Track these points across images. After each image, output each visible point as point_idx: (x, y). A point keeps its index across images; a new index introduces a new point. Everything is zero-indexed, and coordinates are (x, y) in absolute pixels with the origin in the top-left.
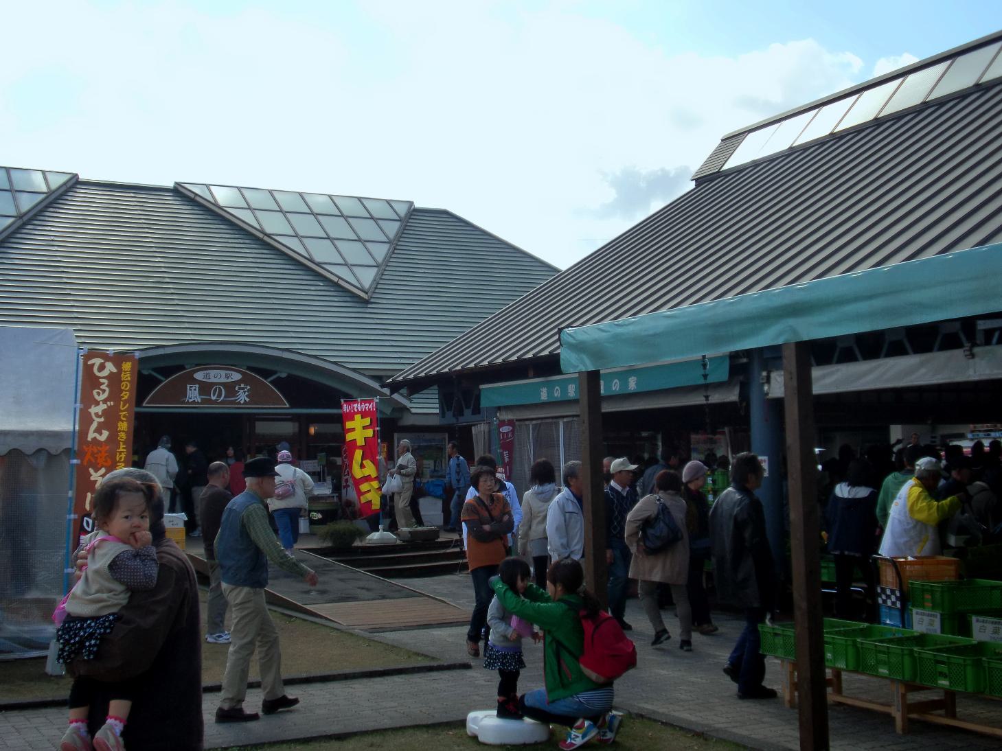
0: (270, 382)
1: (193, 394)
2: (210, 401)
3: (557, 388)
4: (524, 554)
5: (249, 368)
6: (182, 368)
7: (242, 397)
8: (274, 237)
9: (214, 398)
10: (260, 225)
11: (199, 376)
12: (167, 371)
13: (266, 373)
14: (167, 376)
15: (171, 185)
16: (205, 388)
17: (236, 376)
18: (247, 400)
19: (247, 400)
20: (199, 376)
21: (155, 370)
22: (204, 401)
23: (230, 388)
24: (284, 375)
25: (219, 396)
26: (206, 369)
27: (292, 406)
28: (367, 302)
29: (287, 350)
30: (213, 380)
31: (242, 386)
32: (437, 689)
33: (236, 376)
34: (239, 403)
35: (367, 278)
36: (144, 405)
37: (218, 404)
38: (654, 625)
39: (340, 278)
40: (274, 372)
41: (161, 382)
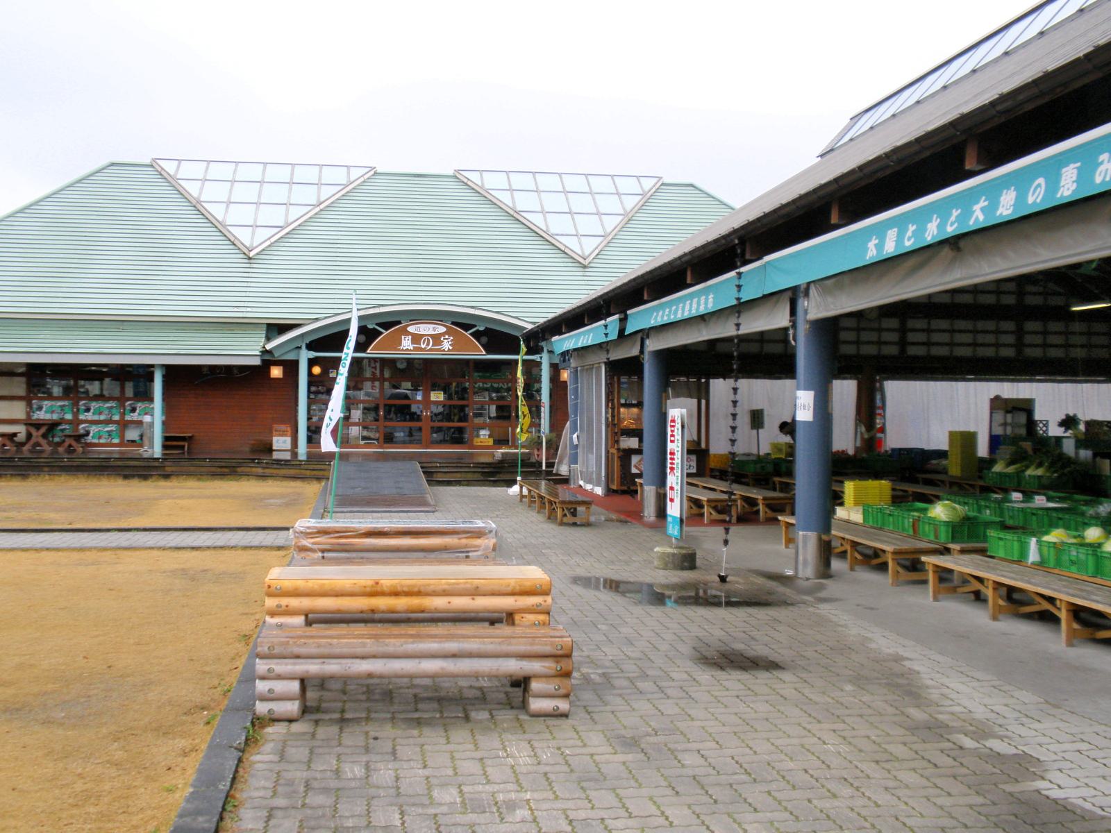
0: (471, 334)
1: (407, 343)
2: (421, 349)
3: (1041, 181)
4: (472, 730)
5: (453, 323)
6: (399, 323)
7: (446, 345)
8: (556, 237)
9: (423, 346)
10: (547, 226)
11: (411, 329)
12: (387, 326)
13: (466, 327)
14: (386, 330)
15: (451, 172)
16: (416, 338)
17: (442, 329)
18: (451, 348)
19: (451, 348)
20: (411, 329)
21: (377, 324)
22: (415, 349)
23: (437, 338)
24: (482, 329)
25: (428, 345)
26: (417, 324)
27: (488, 352)
28: (585, 267)
29: (472, 307)
30: (422, 332)
31: (447, 337)
32: (544, 544)
33: (442, 329)
34: (444, 350)
35: (588, 247)
36: (368, 351)
37: (427, 351)
38: (722, 455)
39: (566, 247)
40: (474, 326)
41: (381, 333)
